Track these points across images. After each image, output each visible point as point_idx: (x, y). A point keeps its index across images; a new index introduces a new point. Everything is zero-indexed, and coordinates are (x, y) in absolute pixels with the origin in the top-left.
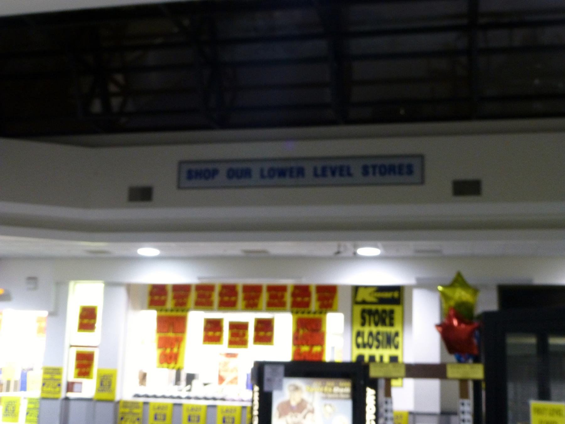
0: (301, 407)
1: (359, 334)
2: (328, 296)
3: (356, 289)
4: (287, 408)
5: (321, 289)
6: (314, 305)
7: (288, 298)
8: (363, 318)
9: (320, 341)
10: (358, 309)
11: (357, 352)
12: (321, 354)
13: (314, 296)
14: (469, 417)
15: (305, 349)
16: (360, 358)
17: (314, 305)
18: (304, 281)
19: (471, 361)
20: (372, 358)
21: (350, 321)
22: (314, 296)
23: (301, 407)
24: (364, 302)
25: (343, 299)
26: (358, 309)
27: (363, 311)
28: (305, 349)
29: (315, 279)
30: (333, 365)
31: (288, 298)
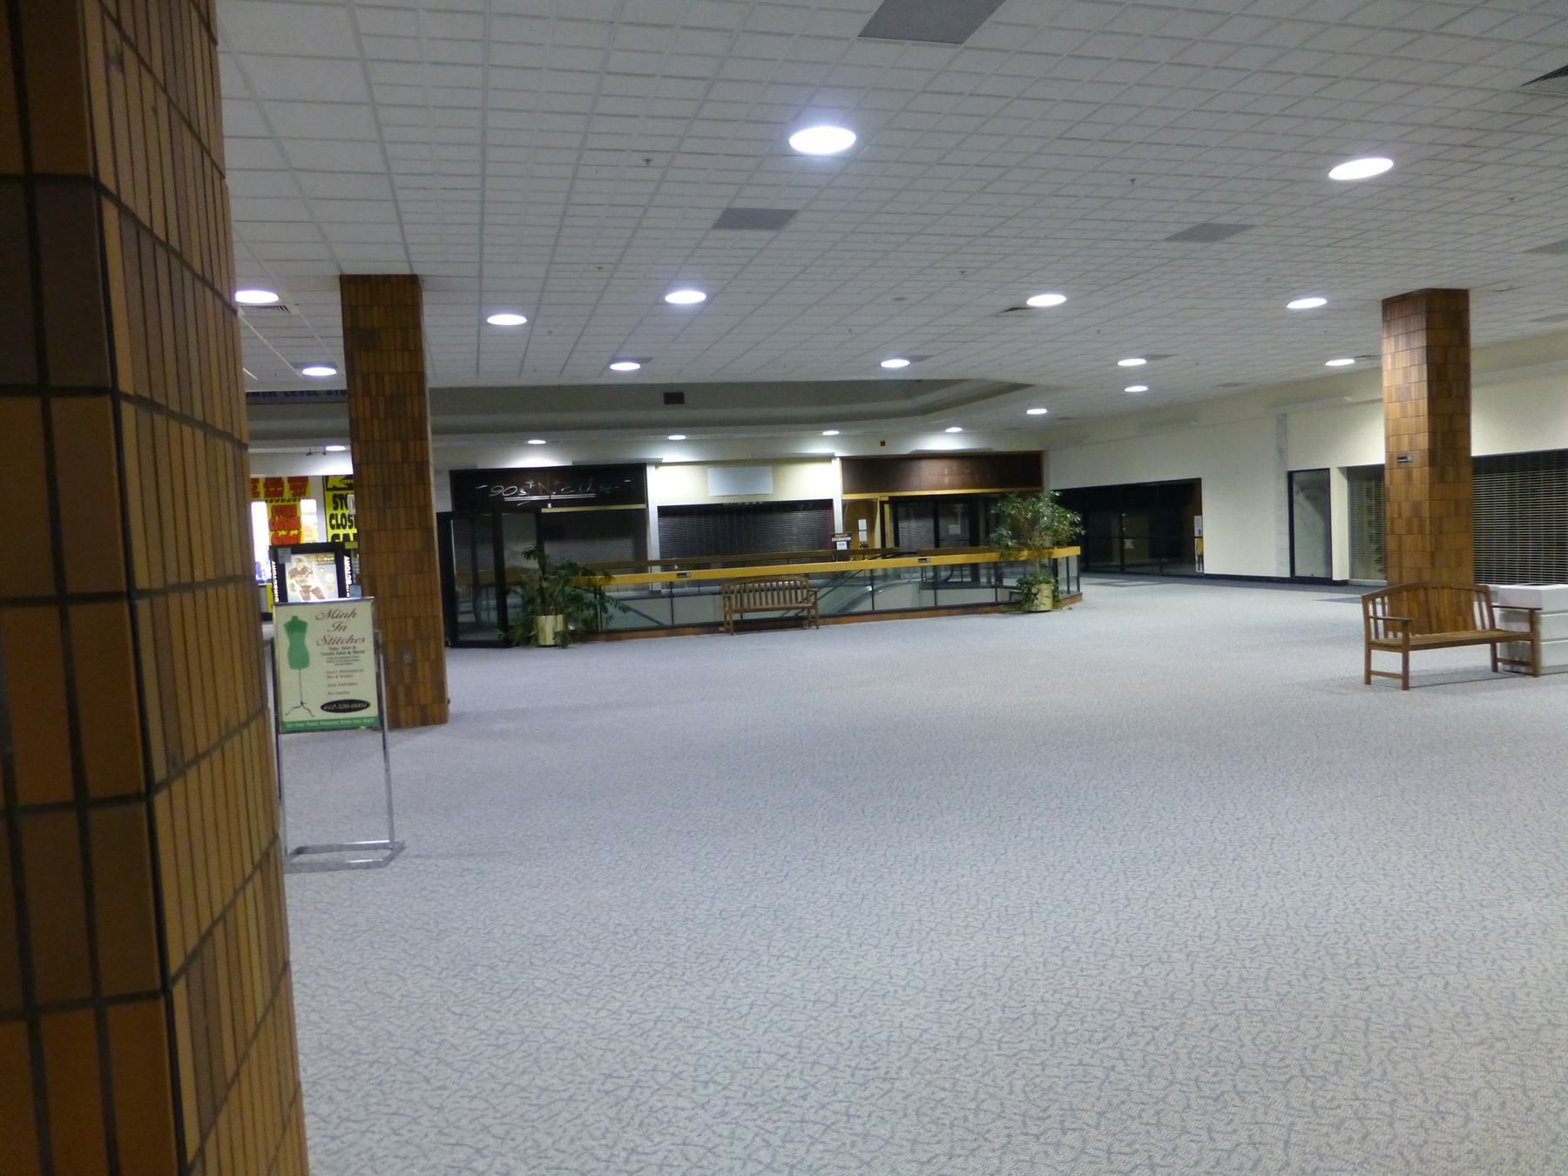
0: (304, 571)
1: (332, 517)
2: (300, 486)
3: (326, 478)
4: (295, 573)
5: (291, 480)
6: (287, 494)
7: (261, 488)
8: (335, 502)
9: (297, 525)
10: (330, 495)
11: (332, 532)
12: (298, 536)
13: (287, 486)
14: (176, 1173)
15: (283, 533)
16: (336, 536)
17: (287, 494)
18: (278, 475)
19: (1197, 518)
20: (346, 537)
21: (323, 505)
22: (287, 486)
23: (304, 571)
24: (334, 488)
25: (313, 487)
26: (330, 495)
27: (335, 496)
28: (283, 533)
29: (285, 472)
30: (919, 516)
31: (261, 488)
